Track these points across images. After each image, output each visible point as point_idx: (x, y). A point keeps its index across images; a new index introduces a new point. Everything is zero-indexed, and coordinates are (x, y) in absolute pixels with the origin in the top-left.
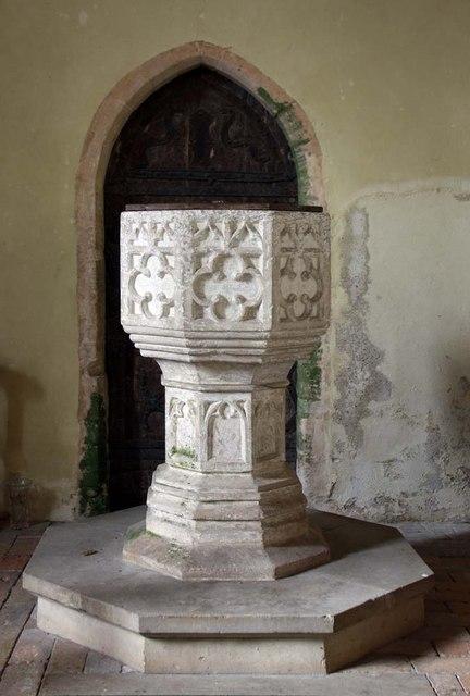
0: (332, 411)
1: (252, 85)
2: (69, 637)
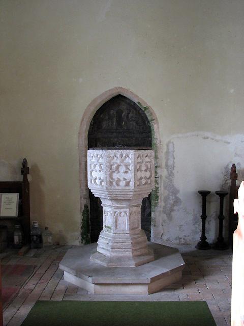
0: (162, 209)
1: (136, 101)
2: (73, 283)
